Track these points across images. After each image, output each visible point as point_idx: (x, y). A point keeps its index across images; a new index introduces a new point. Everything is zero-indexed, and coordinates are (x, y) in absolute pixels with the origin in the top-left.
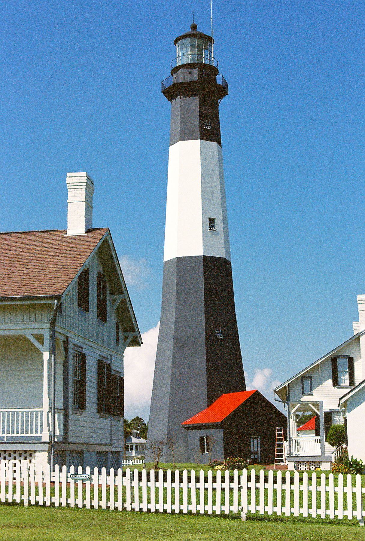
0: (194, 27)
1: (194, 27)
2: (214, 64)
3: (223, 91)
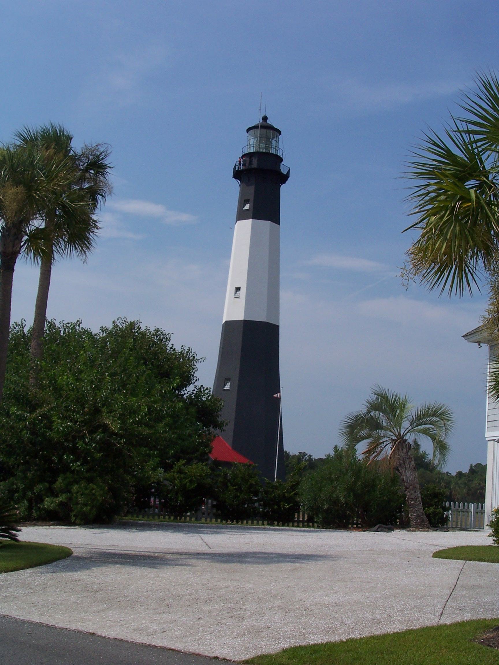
0: (265, 119)
1: (265, 119)
2: (280, 154)
3: (284, 178)
